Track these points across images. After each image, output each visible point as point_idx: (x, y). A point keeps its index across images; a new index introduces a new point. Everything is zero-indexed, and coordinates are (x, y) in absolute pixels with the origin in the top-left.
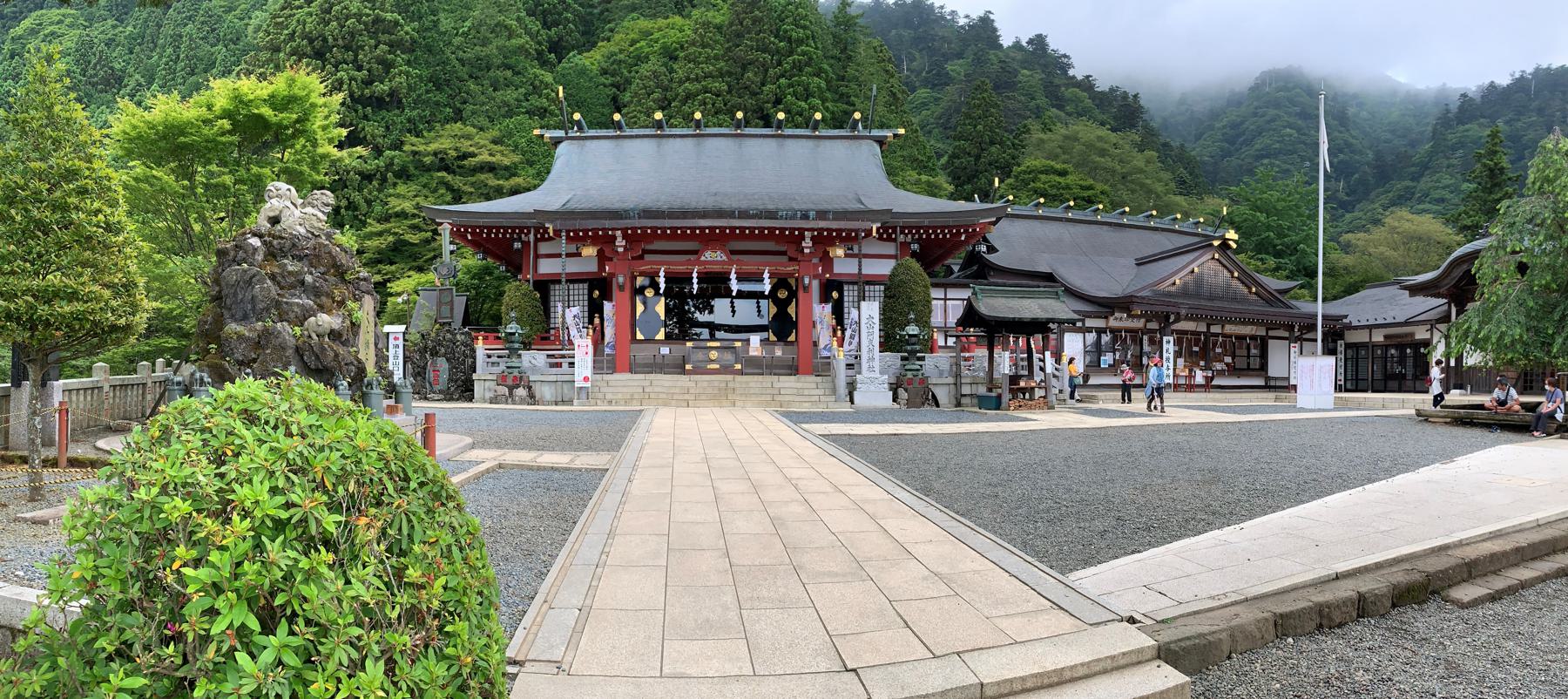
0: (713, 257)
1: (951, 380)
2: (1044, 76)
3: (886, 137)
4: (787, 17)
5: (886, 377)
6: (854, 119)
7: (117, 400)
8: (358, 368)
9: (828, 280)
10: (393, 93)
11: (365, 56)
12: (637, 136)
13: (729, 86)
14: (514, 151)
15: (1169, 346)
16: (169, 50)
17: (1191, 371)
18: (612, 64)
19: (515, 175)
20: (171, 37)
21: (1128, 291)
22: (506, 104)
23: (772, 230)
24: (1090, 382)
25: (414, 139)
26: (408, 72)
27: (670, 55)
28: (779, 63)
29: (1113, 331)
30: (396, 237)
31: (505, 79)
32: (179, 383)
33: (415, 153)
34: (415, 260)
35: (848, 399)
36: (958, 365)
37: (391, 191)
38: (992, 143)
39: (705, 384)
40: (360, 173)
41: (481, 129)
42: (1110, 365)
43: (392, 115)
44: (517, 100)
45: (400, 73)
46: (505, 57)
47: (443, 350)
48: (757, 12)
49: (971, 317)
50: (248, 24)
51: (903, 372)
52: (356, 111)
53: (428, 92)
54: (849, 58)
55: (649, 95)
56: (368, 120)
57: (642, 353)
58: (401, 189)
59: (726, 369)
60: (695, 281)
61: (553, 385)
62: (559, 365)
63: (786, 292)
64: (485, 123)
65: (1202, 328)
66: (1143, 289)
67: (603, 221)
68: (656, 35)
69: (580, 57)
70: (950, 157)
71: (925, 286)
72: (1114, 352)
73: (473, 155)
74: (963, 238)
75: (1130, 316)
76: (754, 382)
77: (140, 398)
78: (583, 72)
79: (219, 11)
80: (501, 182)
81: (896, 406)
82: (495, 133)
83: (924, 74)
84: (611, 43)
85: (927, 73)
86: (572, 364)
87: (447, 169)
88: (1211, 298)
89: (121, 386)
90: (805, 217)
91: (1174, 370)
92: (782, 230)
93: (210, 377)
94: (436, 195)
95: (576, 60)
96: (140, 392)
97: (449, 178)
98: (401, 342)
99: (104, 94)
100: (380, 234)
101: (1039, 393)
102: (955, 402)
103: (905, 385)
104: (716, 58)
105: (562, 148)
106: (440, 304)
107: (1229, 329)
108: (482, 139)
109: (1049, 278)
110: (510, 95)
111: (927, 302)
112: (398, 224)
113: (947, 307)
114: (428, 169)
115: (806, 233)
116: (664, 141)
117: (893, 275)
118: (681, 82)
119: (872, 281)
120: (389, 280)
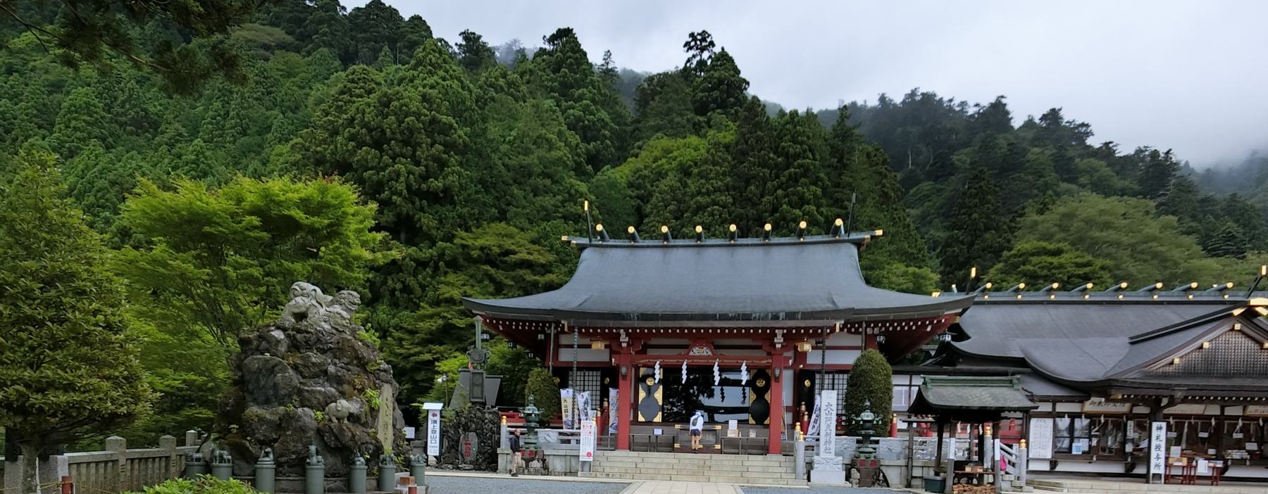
0: (701, 352)
1: (902, 462)
2: (1054, 151)
3: (864, 239)
4: (785, 135)
5: (841, 458)
6: (836, 226)
7: (136, 472)
8: (376, 446)
9: (801, 370)
10: (446, 190)
11: (423, 153)
12: (648, 247)
13: (734, 199)
14: (550, 251)
15: (1159, 433)
16: (218, 104)
17: (1190, 460)
18: (637, 179)
19: (550, 272)
20: (219, 91)
21: (1110, 375)
22: (544, 208)
23: (748, 329)
24: (1058, 469)
25: (464, 234)
26: (460, 172)
27: (685, 171)
28: (777, 177)
29: (1088, 416)
30: (445, 321)
31: (545, 186)
32: (198, 459)
33: (464, 246)
34: (460, 343)
35: (806, 477)
36: (910, 449)
37: (443, 278)
38: (987, 229)
39: (687, 461)
40: (415, 260)
41: (522, 229)
42: (1084, 453)
43: (445, 210)
44: (554, 206)
45: (453, 172)
46: (545, 167)
47: (474, 426)
48: (759, 133)
49: (920, 406)
50: (307, 95)
51: (857, 454)
52: (413, 203)
53: (477, 192)
54: (845, 166)
55: (666, 207)
56: (424, 213)
57: (641, 434)
58: (451, 277)
59: (707, 449)
60: (684, 372)
61: (563, 458)
62: (569, 442)
63: (762, 379)
64: (527, 225)
65: (1214, 410)
66: (1130, 370)
67: (609, 321)
68: (675, 153)
69: (612, 171)
70: (943, 247)
71: (888, 376)
72: (1090, 437)
73: (514, 253)
74: (929, 329)
75: (1108, 400)
76: (728, 460)
77: (163, 471)
78: (613, 185)
79: (277, 75)
80: (537, 278)
81: (849, 484)
82: (533, 234)
83: (928, 168)
84: (639, 159)
85: (932, 166)
86: (578, 442)
87: (493, 264)
88: (1227, 375)
89: (140, 459)
90: (775, 317)
91: (1167, 459)
92: (756, 329)
93: (230, 454)
94: (482, 285)
95: (609, 173)
96: (163, 464)
97: (492, 271)
98: (438, 418)
99: (134, 138)
100: (431, 317)
101: (989, 478)
102: (905, 483)
103: (858, 466)
104: (724, 174)
105: (586, 254)
106: (473, 385)
107: (1253, 410)
108: (523, 238)
109: (1021, 363)
110: (548, 201)
111: (888, 390)
112: (447, 309)
113: (902, 392)
114: (476, 261)
115: (777, 331)
116: (670, 250)
117: (856, 366)
118: (693, 196)
119: (841, 370)
120: (438, 360)
